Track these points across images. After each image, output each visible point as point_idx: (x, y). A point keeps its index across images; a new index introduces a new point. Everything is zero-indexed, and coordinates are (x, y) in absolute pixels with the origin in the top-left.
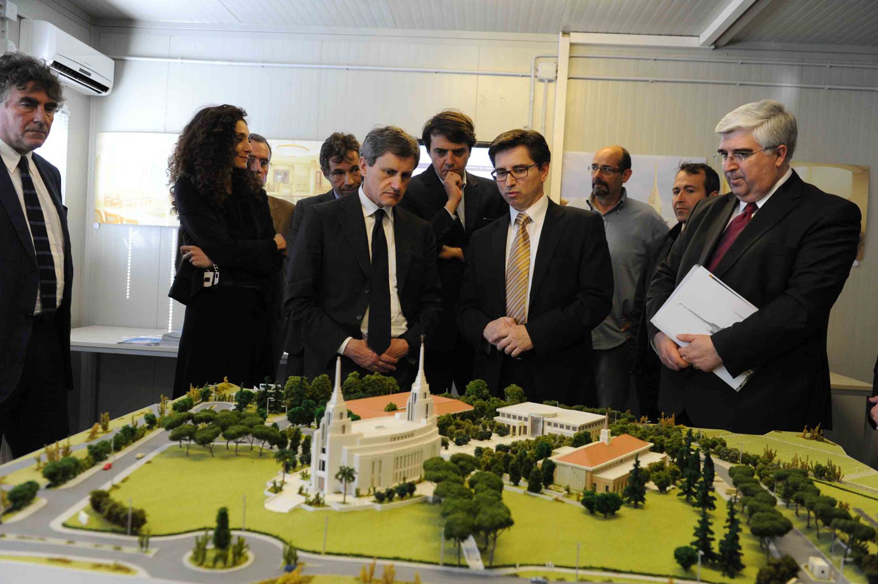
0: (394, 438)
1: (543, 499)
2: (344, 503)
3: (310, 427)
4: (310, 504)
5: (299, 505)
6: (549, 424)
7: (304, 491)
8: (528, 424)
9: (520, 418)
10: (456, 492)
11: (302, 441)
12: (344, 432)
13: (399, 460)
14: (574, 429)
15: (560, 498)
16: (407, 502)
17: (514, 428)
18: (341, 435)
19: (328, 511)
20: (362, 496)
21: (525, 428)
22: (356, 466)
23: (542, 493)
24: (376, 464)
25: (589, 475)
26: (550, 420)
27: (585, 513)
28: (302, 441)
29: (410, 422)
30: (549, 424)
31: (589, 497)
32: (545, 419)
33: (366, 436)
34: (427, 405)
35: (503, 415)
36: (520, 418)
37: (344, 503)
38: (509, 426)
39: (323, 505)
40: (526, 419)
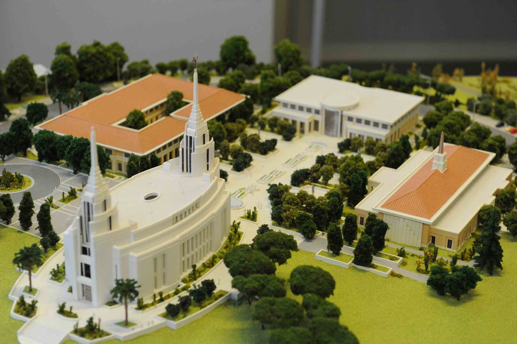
0: (176, 218)
1: (376, 275)
2: (126, 324)
3: (25, 155)
4: (81, 333)
5: (68, 336)
6: (350, 119)
7: (67, 309)
8: (321, 118)
9: (309, 110)
10: (283, 314)
11: (37, 210)
12: (111, 229)
13: (185, 245)
14: (385, 126)
15: (397, 272)
16: (210, 306)
17: (302, 124)
18: (110, 232)
19: (110, 341)
20: (146, 306)
21: (316, 123)
22: (133, 275)
23: (373, 266)
24: (159, 260)
25: (427, 228)
26: (351, 113)
27: (432, 296)
28: (37, 210)
29: (186, 174)
30: (350, 119)
31: (438, 276)
32: (346, 113)
33: (140, 227)
34: (208, 150)
35: (285, 105)
36: (309, 110)
37: (126, 324)
38: (294, 122)
39: (102, 334)
40: (317, 112)
